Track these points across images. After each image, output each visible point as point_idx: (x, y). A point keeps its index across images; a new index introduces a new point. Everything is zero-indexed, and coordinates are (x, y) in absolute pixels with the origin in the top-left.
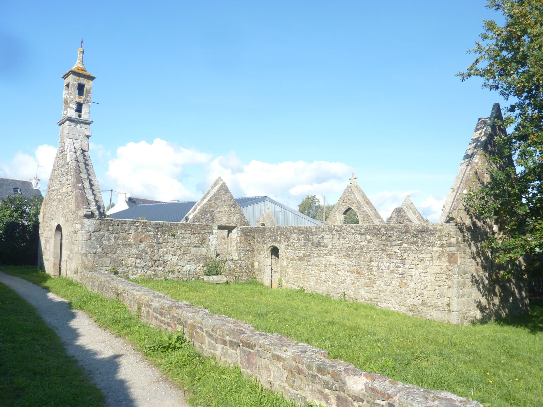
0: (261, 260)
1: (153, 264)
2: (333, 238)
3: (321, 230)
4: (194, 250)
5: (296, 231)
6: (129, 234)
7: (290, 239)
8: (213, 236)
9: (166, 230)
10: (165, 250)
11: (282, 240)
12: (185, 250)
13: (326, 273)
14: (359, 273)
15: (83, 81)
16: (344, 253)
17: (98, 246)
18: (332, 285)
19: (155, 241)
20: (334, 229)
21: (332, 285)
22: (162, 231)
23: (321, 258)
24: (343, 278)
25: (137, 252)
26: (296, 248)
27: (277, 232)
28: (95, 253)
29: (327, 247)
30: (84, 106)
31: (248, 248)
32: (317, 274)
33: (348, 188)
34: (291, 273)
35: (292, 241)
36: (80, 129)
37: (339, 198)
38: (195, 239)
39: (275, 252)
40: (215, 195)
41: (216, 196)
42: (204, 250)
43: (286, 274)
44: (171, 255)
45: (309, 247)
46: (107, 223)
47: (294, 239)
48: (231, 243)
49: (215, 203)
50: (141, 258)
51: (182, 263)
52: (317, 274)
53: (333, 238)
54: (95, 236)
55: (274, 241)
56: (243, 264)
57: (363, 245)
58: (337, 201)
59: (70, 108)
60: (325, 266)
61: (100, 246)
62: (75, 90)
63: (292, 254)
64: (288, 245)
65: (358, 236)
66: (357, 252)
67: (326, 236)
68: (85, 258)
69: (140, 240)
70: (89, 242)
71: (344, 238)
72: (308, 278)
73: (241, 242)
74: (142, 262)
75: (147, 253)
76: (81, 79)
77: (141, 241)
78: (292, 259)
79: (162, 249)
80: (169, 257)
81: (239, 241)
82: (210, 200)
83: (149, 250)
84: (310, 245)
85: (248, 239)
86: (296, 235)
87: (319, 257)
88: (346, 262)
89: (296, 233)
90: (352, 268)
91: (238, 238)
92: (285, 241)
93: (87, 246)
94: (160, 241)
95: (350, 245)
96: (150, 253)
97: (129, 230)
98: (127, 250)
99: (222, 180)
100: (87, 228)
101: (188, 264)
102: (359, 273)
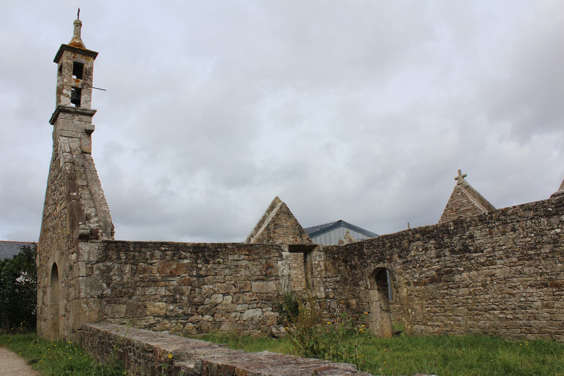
0: (362, 295)
1: (194, 309)
2: (491, 234)
3: (465, 225)
4: (256, 286)
5: (418, 235)
6: (151, 264)
7: (409, 251)
8: (284, 262)
9: (210, 256)
10: (211, 287)
11: (396, 256)
12: (242, 285)
13: (487, 297)
14: (557, 286)
15: (80, 59)
16: (518, 254)
17: (105, 285)
18: (502, 316)
19: (194, 274)
20: (491, 218)
21: (502, 316)
22: (204, 256)
23: (474, 273)
24: (522, 299)
25: (168, 293)
26: (422, 264)
27: (384, 245)
28: (101, 297)
29: (482, 251)
30: (83, 91)
31: (338, 278)
32: (470, 301)
33: (456, 191)
34: (418, 307)
35: (413, 253)
36: (78, 123)
37: (444, 207)
38: (256, 269)
39: (381, 277)
40: (273, 221)
41: (275, 223)
42: (272, 286)
43: (410, 310)
44: (221, 295)
45: (447, 258)
46: (117, 247)
47: (417, 249)
48: (312, 273)
49: (274, 232)
50: (175, 302)
51: (239, 308)
52: (470, 301)
53: (491, 234)
54: (99, 268)
55: (380, 260)
56: (334, 305)
57: (557, 234)
58: (443, 212)
59: (64, 95)
60: (484, 285)
61: (108, 285)
62: (69, 71)
63: (417, 275)
64: (407, 262)
65: (544, 220)
66: (546, 249)
67: (477, 234)
68: (85, 306)
69: (171, 272)
70: (90, 280)
71: (514, 230)
72: (451, 311)
73: (326, 269)
74: (177, 309)
75: (182, 294)
76: (78, 56)
77: (172, 275)
78: (416, 284)
79: (206, 286)
80: (219, 298)
81: (323, 268)
82: (267, 228)
83: (186, 289)
84: (447, 253)
85: (337, 264)
86: (420, 243)
87: (470, 270)
88: (526, 270)
89: (419, 240)
90: (539, 278)
91: (322, 264)
92: (400, 257)
93: (86, 286)
94: (202, 273)
95: (529, 239)
96: (187, 293)
97: (152, 256)
98: (150, 291)
99: (280, 201)
100: (86, 257)
101: (248, 309)
102: (557, 286)
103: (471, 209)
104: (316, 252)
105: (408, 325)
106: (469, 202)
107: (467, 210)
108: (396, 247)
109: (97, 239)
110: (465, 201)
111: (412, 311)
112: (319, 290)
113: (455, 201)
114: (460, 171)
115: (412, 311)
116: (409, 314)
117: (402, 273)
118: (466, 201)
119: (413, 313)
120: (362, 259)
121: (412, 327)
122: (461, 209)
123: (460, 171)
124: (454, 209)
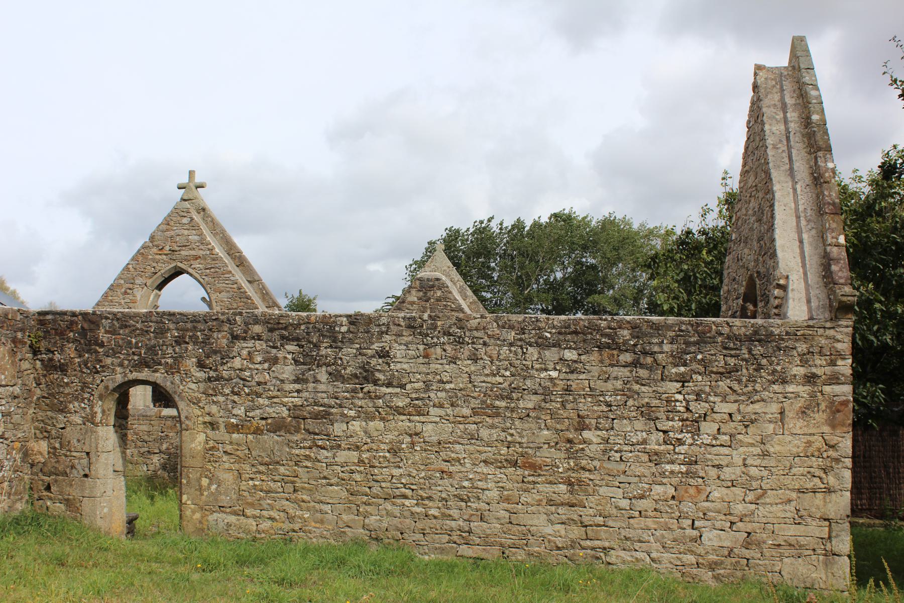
103: (204, 258)
107: (196, 258)
113: (172, 233)
114: (191, 173)
118: (196, 238)
122: (183, 253)
123: (191, 173)
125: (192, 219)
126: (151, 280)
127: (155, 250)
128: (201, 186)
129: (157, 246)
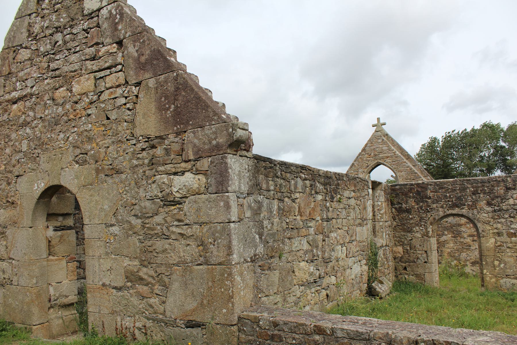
11: (482, 204)
92: (489, 204)
103: (392, 157)
104: (379, 191)
105: (491, 278)
106: (390, 149)
107: (387, 157)
108: (484, 193)
109: (248, 151)
110: (385, 148)
111: (500, 264)
112: (382, 237)
113: (374, 147)
114: (378, 119)
115: (500, 264)
116: (494, 266)
117: (490, 222)
118: (386, 148)
119: (502, 265)
120: (422, 202)
121: (497, 280)
122: (380, 155)
123: (378, 119)
124: (372, 154)
125: (383, 140)
126: (366, 170)
127: (367, 156)
128: (384, 124)
129: (368, 154)
